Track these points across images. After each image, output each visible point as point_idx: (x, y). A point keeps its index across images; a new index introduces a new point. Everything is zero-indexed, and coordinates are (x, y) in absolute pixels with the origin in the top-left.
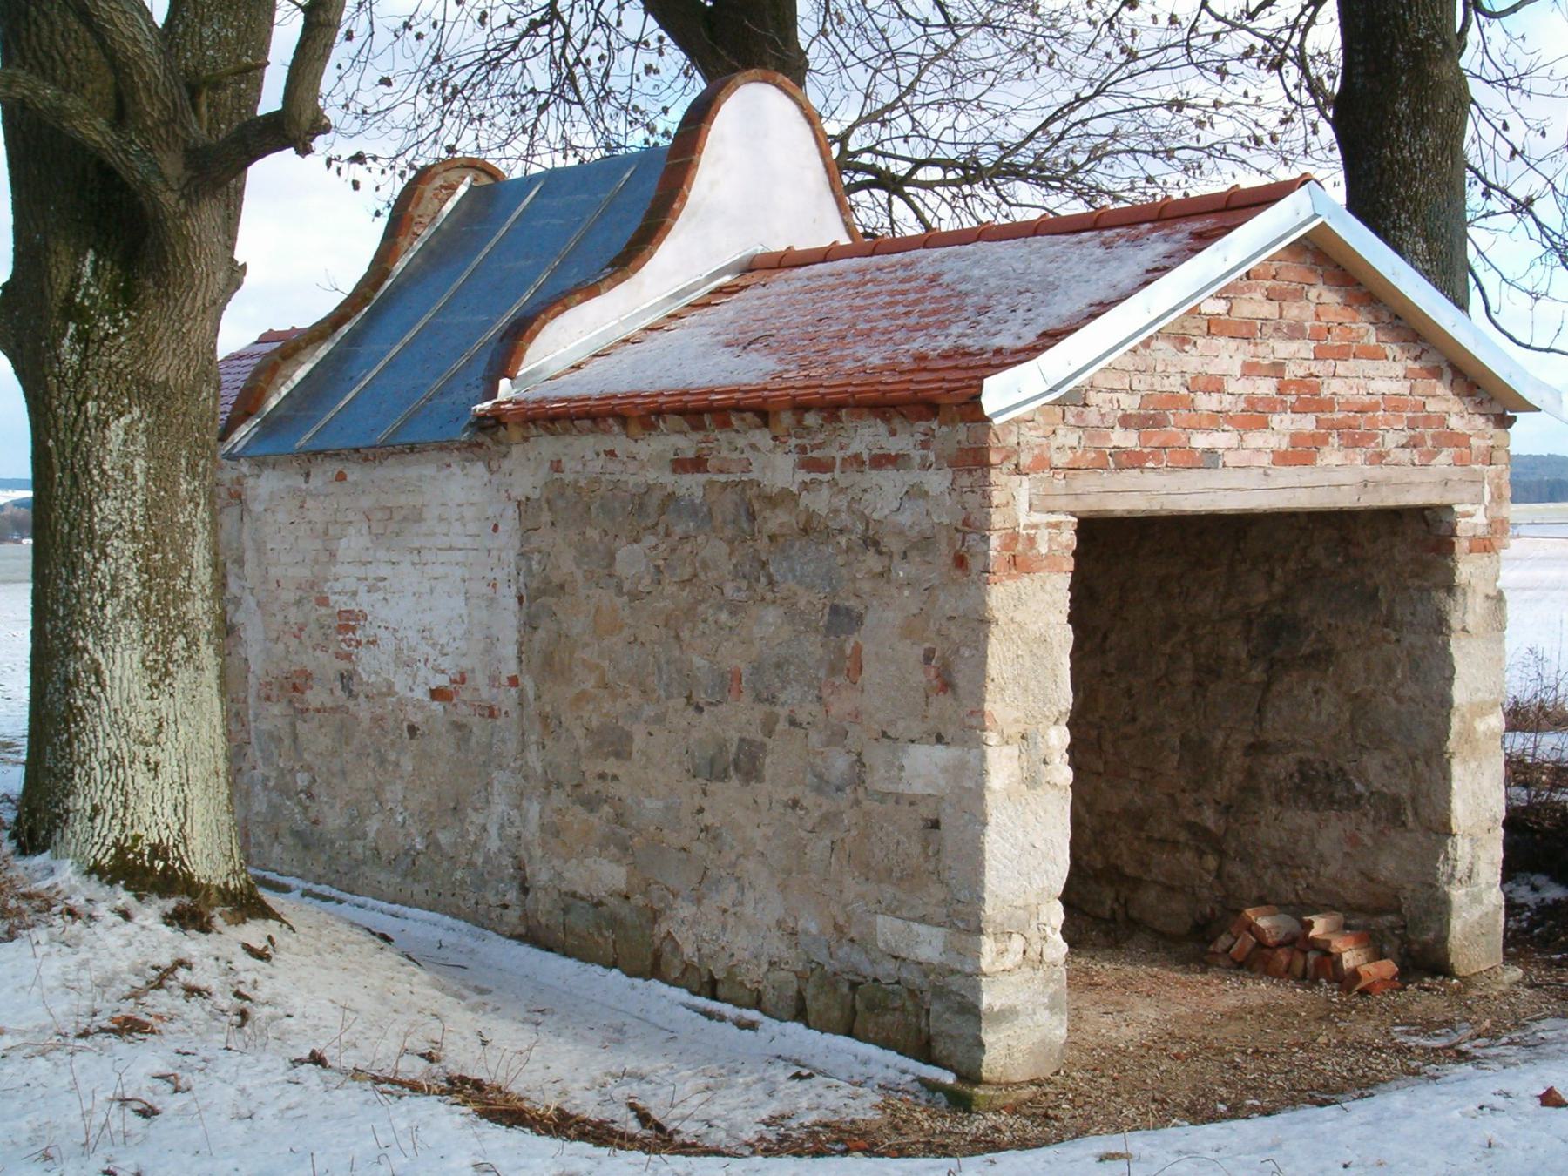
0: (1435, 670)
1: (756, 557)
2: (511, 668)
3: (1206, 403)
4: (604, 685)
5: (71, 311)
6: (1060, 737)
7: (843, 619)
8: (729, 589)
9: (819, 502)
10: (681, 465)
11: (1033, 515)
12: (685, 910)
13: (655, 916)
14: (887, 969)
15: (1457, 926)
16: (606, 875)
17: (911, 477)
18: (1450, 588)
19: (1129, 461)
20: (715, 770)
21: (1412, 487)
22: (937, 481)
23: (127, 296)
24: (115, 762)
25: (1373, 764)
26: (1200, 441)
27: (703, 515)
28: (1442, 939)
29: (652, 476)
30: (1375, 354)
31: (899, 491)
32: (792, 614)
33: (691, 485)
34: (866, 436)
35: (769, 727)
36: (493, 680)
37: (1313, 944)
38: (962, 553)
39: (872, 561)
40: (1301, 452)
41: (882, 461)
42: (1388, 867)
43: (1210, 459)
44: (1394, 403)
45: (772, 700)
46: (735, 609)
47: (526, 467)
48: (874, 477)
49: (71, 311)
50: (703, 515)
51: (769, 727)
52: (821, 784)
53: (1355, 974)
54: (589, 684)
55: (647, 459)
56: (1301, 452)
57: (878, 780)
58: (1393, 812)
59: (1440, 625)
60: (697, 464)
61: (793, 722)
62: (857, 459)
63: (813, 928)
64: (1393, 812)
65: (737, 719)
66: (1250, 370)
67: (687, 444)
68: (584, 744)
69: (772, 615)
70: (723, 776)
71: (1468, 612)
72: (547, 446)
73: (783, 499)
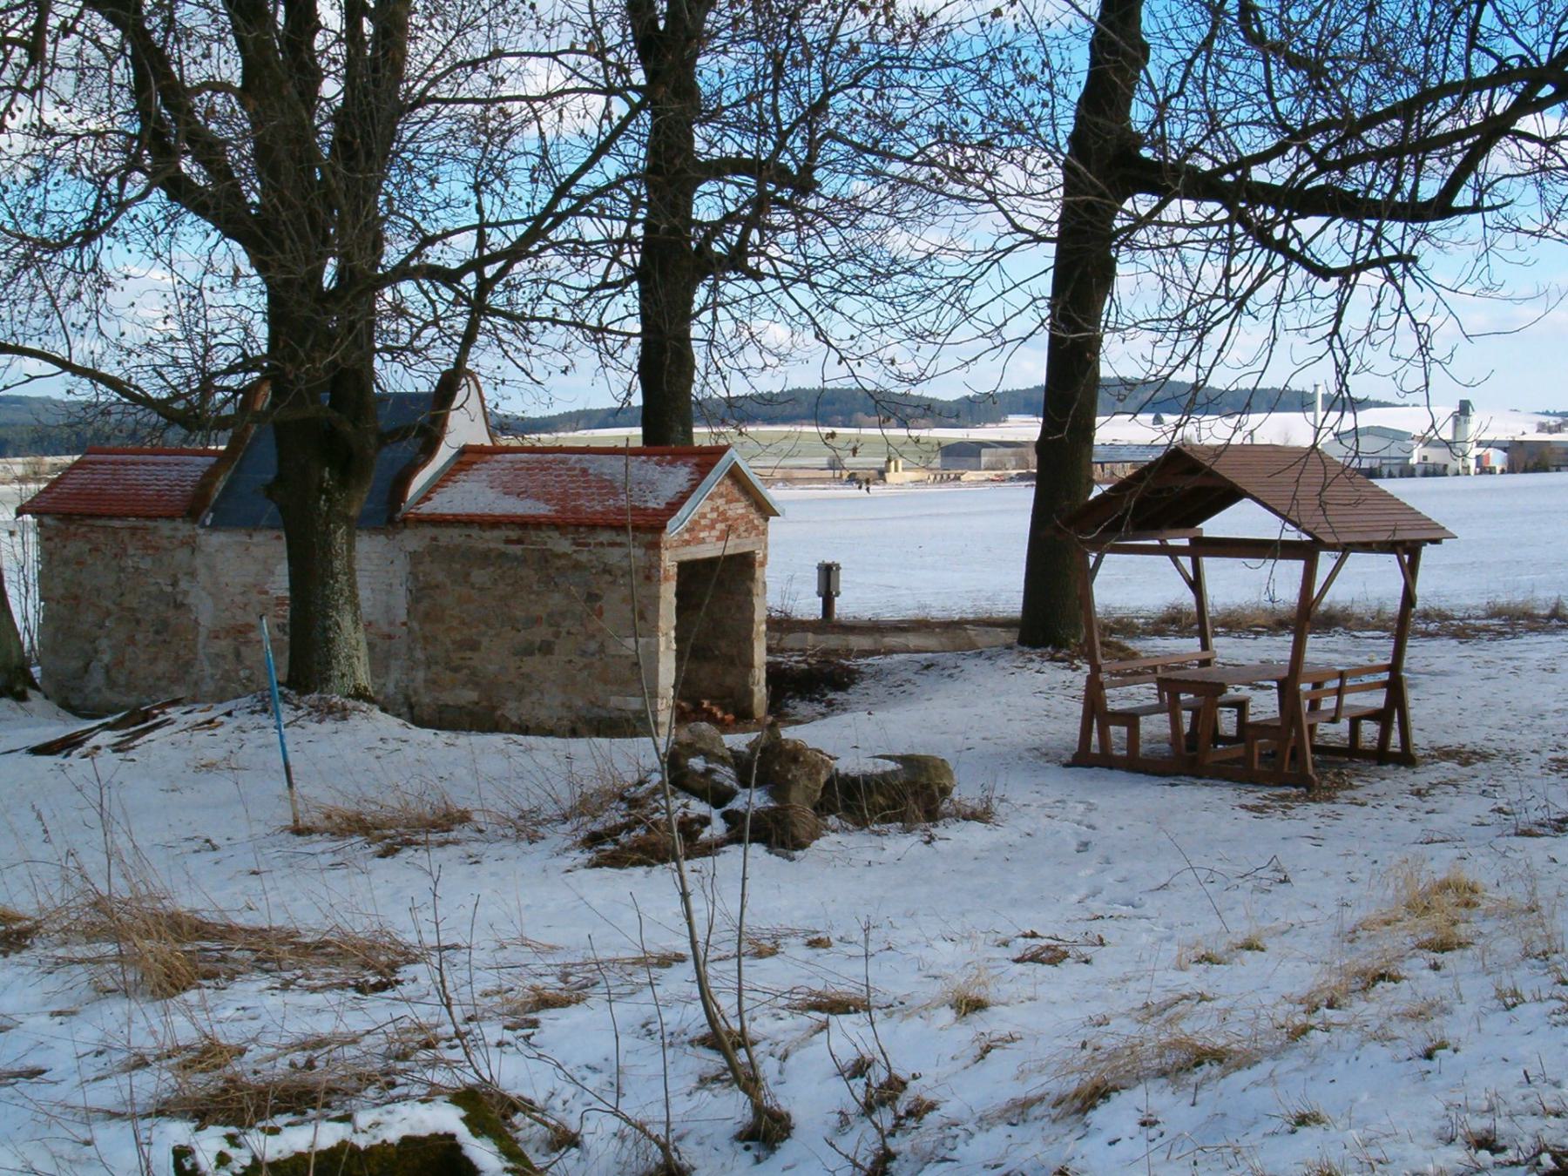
0: (749, 608)
1: (548, 576)
2: (404, 618)
3: (703, 522)
4: (463, 623)
5: (322, 491)
6: (673, 634)
7: (592, 597)
8: (535, 587)
9: (583, 557)
10: (508, 541)
11: (669, 562)
12: (511, 705)
13: (494, 708)
14: (615, 714)
15: (756, 701)
16: (469, 696)
17: (625, 550)
18: (752, 579)
19: (687, 543)
20: (528, 651)
21: (734, 546)
22: (638, 552)
23: (343, 484)
24: (349, 657)
25: (723, 644)
26: (702, 535)
27: (522, 561)
28: (751, 705)
29: (492, 545)
30: (738, 501)
31: (625, 553)
32: (568, 594)
33: (516, 549)
34: (605, 536)
35: (557, 635)
36: (391, 623)
37: (705, 710)
38: (650, 575)
39: (608, 578)
40: (724, 536)
41: (613, 544)
42: (729, 681)
43: (703, 541)
44: (742, 516)
45: (558, 626)
46: (538, 594)
47: (413, 540)
48: (610, 549)
49: (322, 491)
50: (522, 561)
51: (557, 635)
52: (584, 653)
53: (723, 720)
54: (455, 623)
55: (491, 540)
56: (724, 536)
57: (612, 650)
58: (731, 661)
59: (749, 593)
60: (519, 541)
61: (569, 633)
62: (602, 544)
63: (580, 703)
64: (731, 661)
65: (542, 633)
66: (712, 510)
67: (514, 534)
68: (451, 647)
69: (557, 596)
70: (531, 654)
71: (757, 589)
72: (430, 532)
73: (565, 555)
